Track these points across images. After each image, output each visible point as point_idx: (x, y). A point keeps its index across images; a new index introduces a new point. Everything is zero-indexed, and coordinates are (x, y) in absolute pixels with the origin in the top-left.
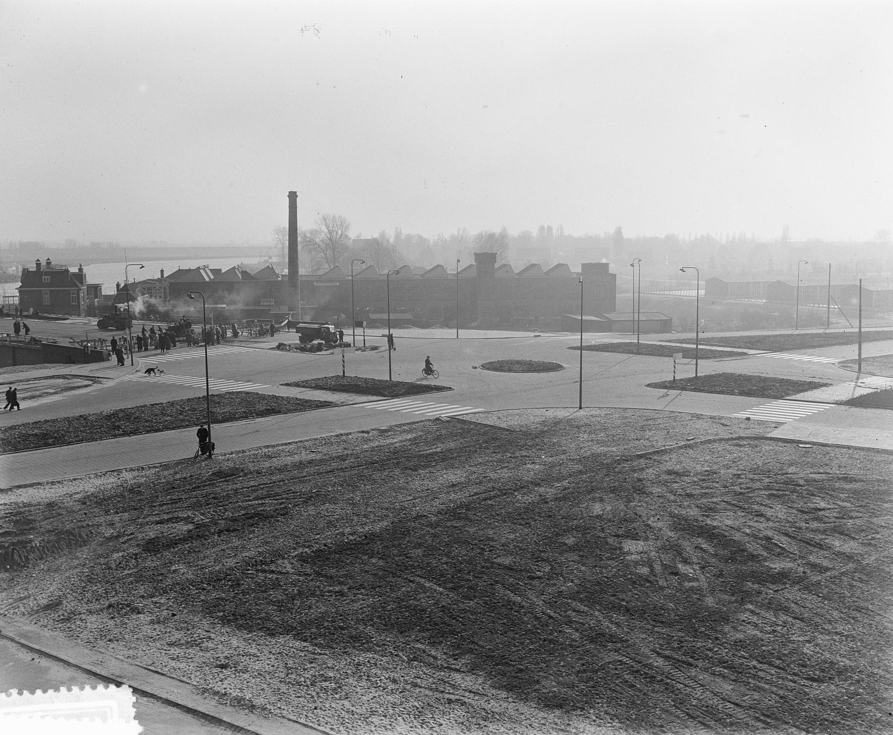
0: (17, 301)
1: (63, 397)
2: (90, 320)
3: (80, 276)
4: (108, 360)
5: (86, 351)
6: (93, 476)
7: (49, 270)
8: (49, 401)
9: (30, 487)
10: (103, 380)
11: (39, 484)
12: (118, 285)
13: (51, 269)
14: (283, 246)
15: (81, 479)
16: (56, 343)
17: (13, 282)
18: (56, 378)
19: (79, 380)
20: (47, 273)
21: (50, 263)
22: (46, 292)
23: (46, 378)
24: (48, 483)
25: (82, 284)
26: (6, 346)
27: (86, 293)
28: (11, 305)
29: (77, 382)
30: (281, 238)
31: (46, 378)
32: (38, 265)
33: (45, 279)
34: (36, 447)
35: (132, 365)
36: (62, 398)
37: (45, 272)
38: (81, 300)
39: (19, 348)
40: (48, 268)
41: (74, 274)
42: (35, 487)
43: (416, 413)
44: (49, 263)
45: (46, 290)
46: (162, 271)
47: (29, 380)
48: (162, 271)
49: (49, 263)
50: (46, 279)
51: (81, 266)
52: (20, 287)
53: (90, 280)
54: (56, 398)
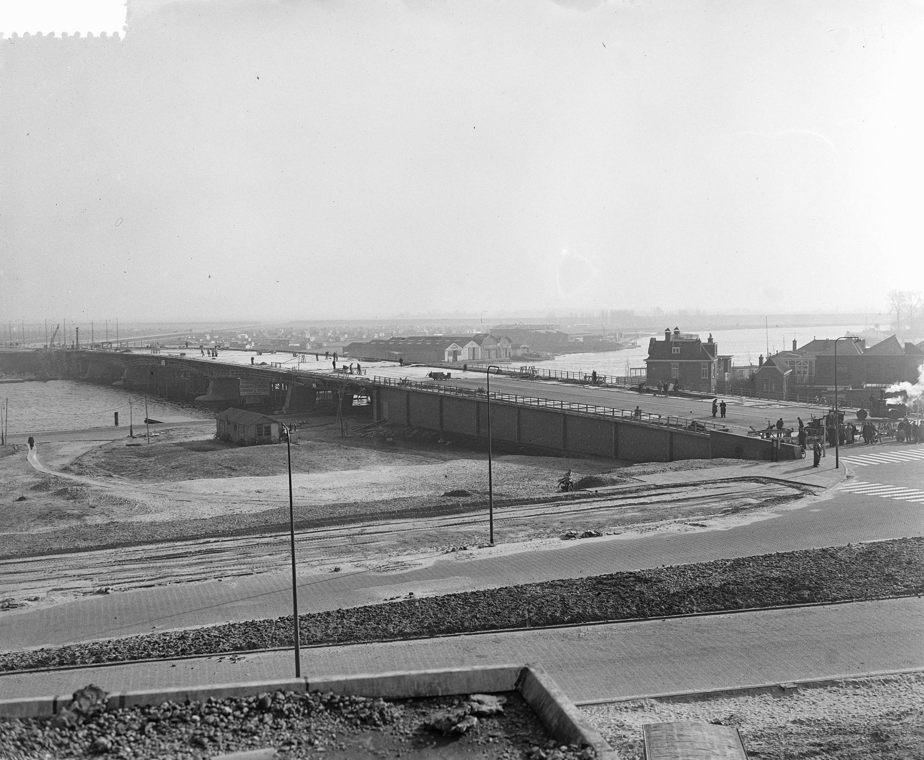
0: (644, 373)
1: (777, 512)
2: (741, 400)
3: (711, 347)
4: (801, 458)
5: (775, 445)
6: (913, 678)
7: (677, 340)
8: (761, 519)
9: (821, 686)
10: (815, 489)
11: (833, 683)
12: (761, 358)
13: (680, 338)
14: (898, 314)
15: (896, 681)
16: (727, 430)
17: (615, 350)
18: (748, 481)
19: (777, 486)
20: (676, 344)
21: (678, 332)
22: (704, 364)
23: (736, 480)
24: (848, 683)
25: (713, 355)
26: (661, 430)
27: (716, 366)
28: (633, 377)
29: (778, 490)
30: (897, 304)
31: (736, 480)
32: (668, 335)
33: (674, 350)
34: (789, 603)
35: (837, 467)
36: (775, 516)
37: (675, 342)
38: (712, 374)
39: (450, 397)
40: (675, 338)
41: (705, 345)
42: (829, 688)
43: (896, 498)
44: (677, 333)
45: (675, 362)
46: (795, 342)
47: (715, 482)
48: (795, 342)
49: (677, 333)
50: (676, 350)
51: (711, 335)
52: (649, 358)
53: (721, 352)
54: (765, 515)
